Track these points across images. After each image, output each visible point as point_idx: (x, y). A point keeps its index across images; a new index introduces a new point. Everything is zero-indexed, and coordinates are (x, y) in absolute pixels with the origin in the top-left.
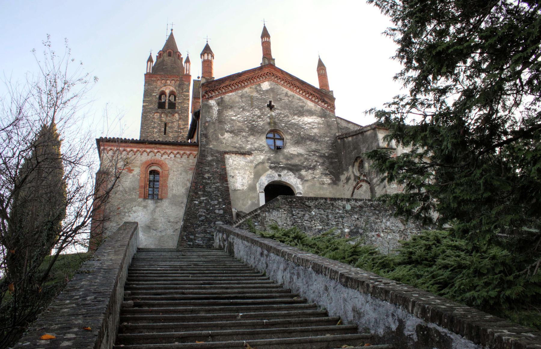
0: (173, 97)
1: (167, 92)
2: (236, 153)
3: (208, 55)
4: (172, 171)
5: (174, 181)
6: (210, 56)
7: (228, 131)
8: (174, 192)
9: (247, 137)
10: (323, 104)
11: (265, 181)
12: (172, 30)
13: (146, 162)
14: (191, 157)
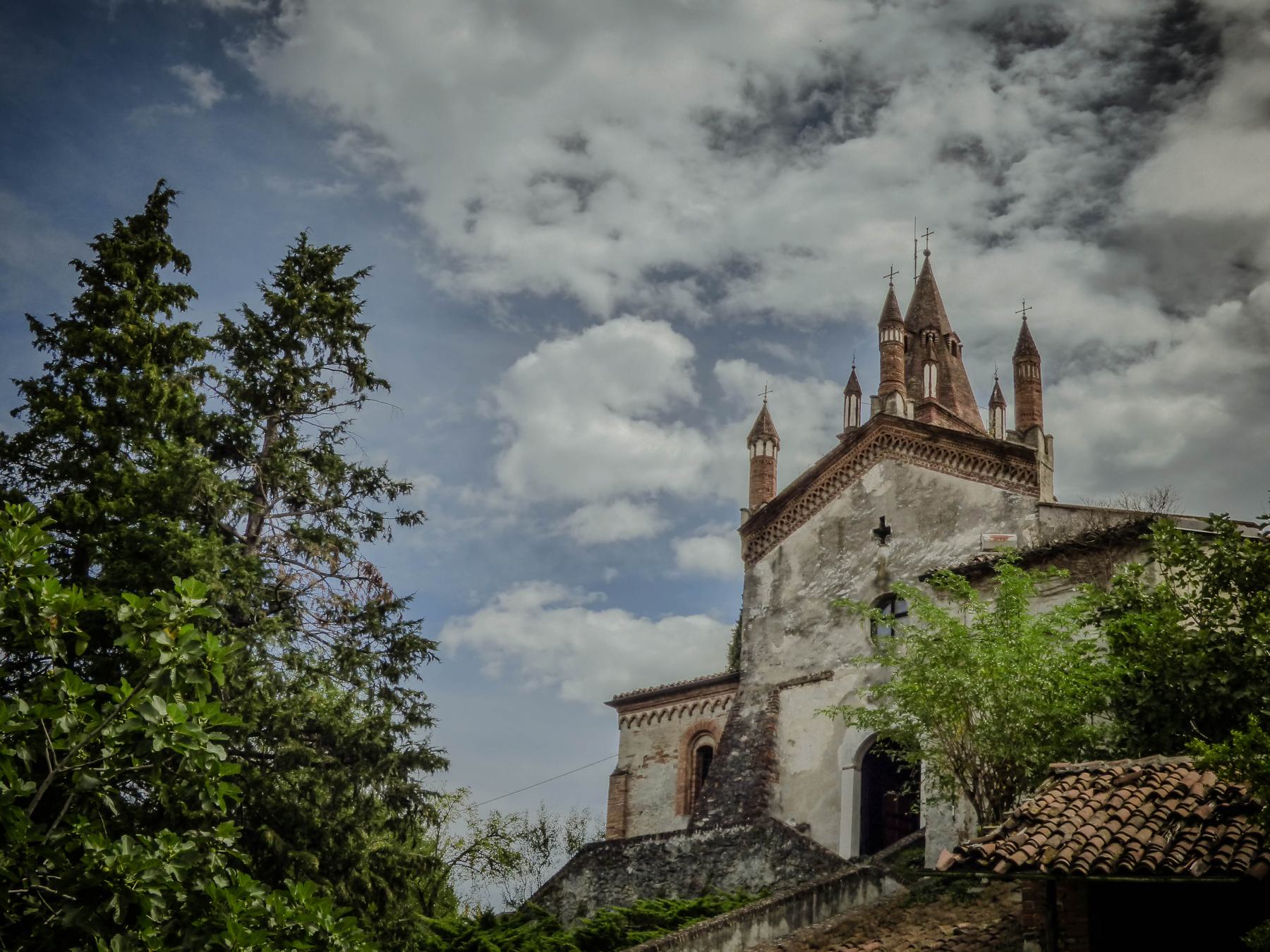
2: (803, 682)
3: (765, 444)
6: (769, 444)
9: (825, 635)
10: (1007, 478)
12: (927, 253)
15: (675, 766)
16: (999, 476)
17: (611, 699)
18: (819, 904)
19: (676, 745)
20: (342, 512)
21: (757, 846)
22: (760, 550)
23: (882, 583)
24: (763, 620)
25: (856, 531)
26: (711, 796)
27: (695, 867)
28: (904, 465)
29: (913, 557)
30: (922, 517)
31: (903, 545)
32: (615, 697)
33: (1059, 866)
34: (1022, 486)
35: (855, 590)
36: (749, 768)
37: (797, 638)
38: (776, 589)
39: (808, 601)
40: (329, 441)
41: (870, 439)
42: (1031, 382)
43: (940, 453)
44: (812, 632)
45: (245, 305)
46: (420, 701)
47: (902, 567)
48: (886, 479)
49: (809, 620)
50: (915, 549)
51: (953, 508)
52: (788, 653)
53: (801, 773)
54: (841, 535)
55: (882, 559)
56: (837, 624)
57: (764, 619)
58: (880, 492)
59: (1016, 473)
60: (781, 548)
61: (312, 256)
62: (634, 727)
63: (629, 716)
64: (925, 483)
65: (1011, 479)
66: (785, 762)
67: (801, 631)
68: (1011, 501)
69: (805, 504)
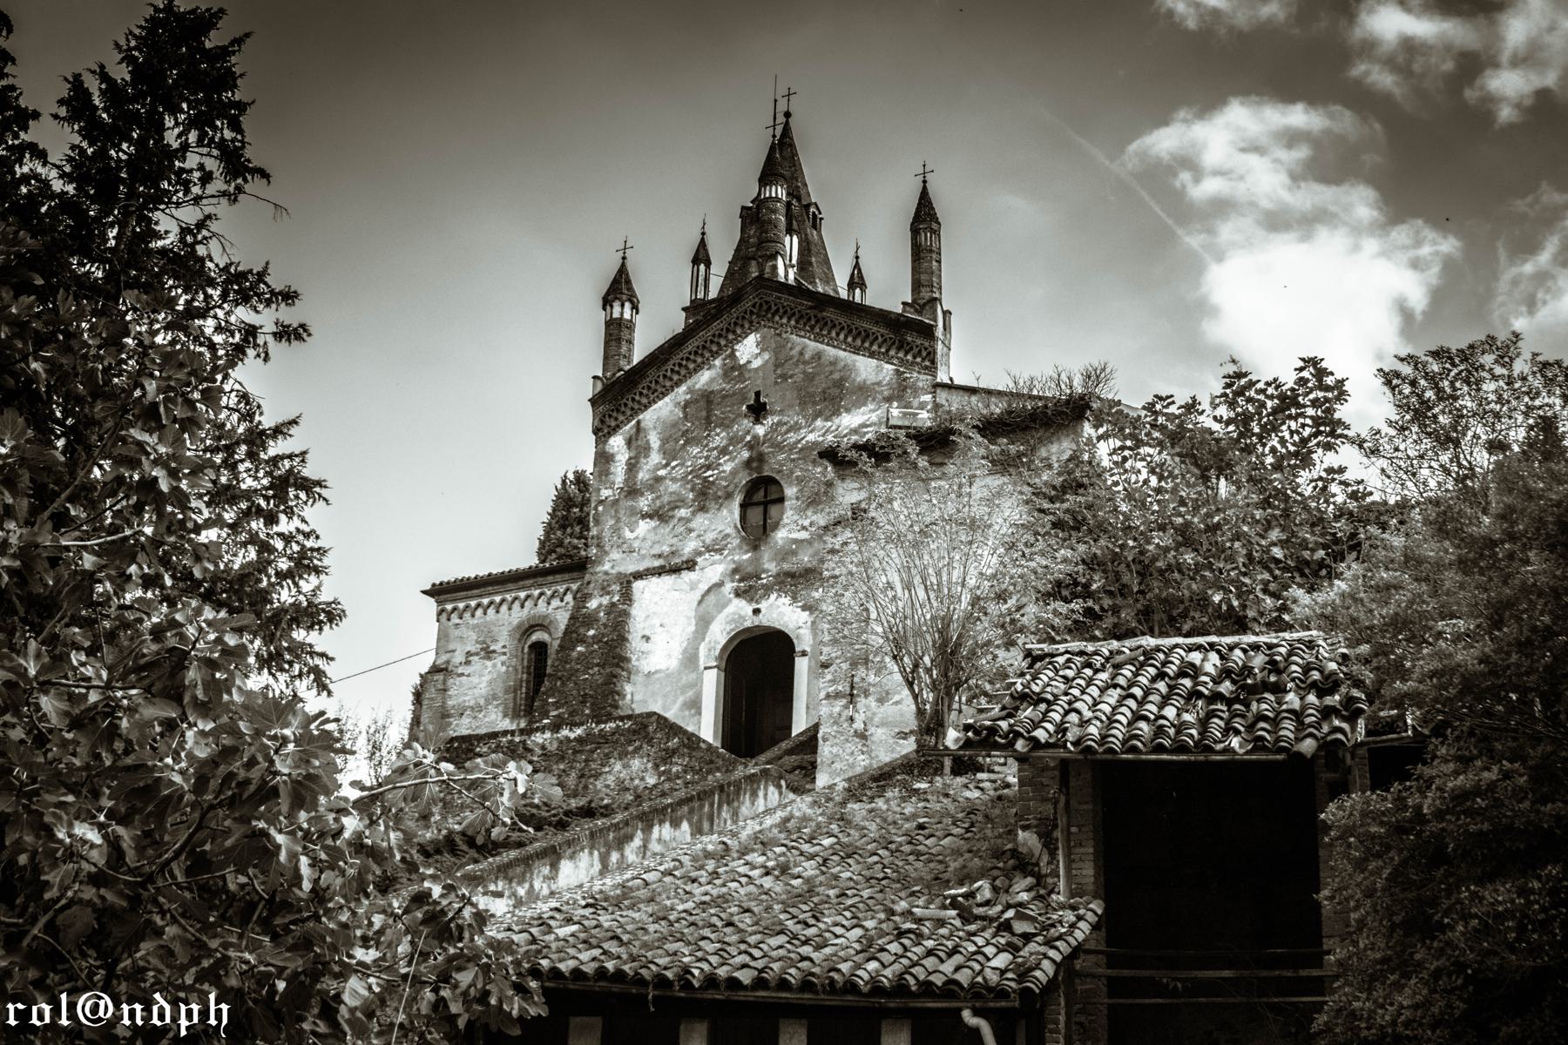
2: (659, 572)
6: (627, 305)
9: (688, 520)
11: (719, 634)
12: (787, 115)
13: (519, 626)
15: (503, 664)
16: (892, 353)
17: (428, 587)
18: (720, 806)
19: (503, 641)
20: (209, 325)
21: (637, 743)
22: (613, 424)
23: (755, 465)
24: (616, 502)
25: (726, 406)
26: (553, 696)
27: (562, 767)
28: (784, 336)
29: (792, 437)
30: (803, 393)
31: (780, 424)
32: (434, 585)
33: (1089, 743)
34: (918, 364)
35: (724, 471)
36: (598, 665)
37: (653, 523)
38: (632, 467)
39: (668, 482)
40: (189, 239)
41: (747, 304)
42: (931, 251)
43: (826, 323)
44: (673, 517)
45: (102, 67)
46: (309, 544)
47: (779, 447)
48: (763, 350)
49: (669, 503)
50: (796, 428)
51: (839, 384)
52: (644, 539)
53: (656, 672)
54: (709, 411)
55: (755, 437)
56: (702, 509)
57: (617, 500)
58: (756, 364)
59: (911, 349)
60: (639, 422)
61: (181, 17)
62: (455, 619)
63: (449, 607)
64: (807, 356)
65: (906, 355)
66: (638, 660)
67: (659, 515)
68: (905, 380)
69: (669, 374)
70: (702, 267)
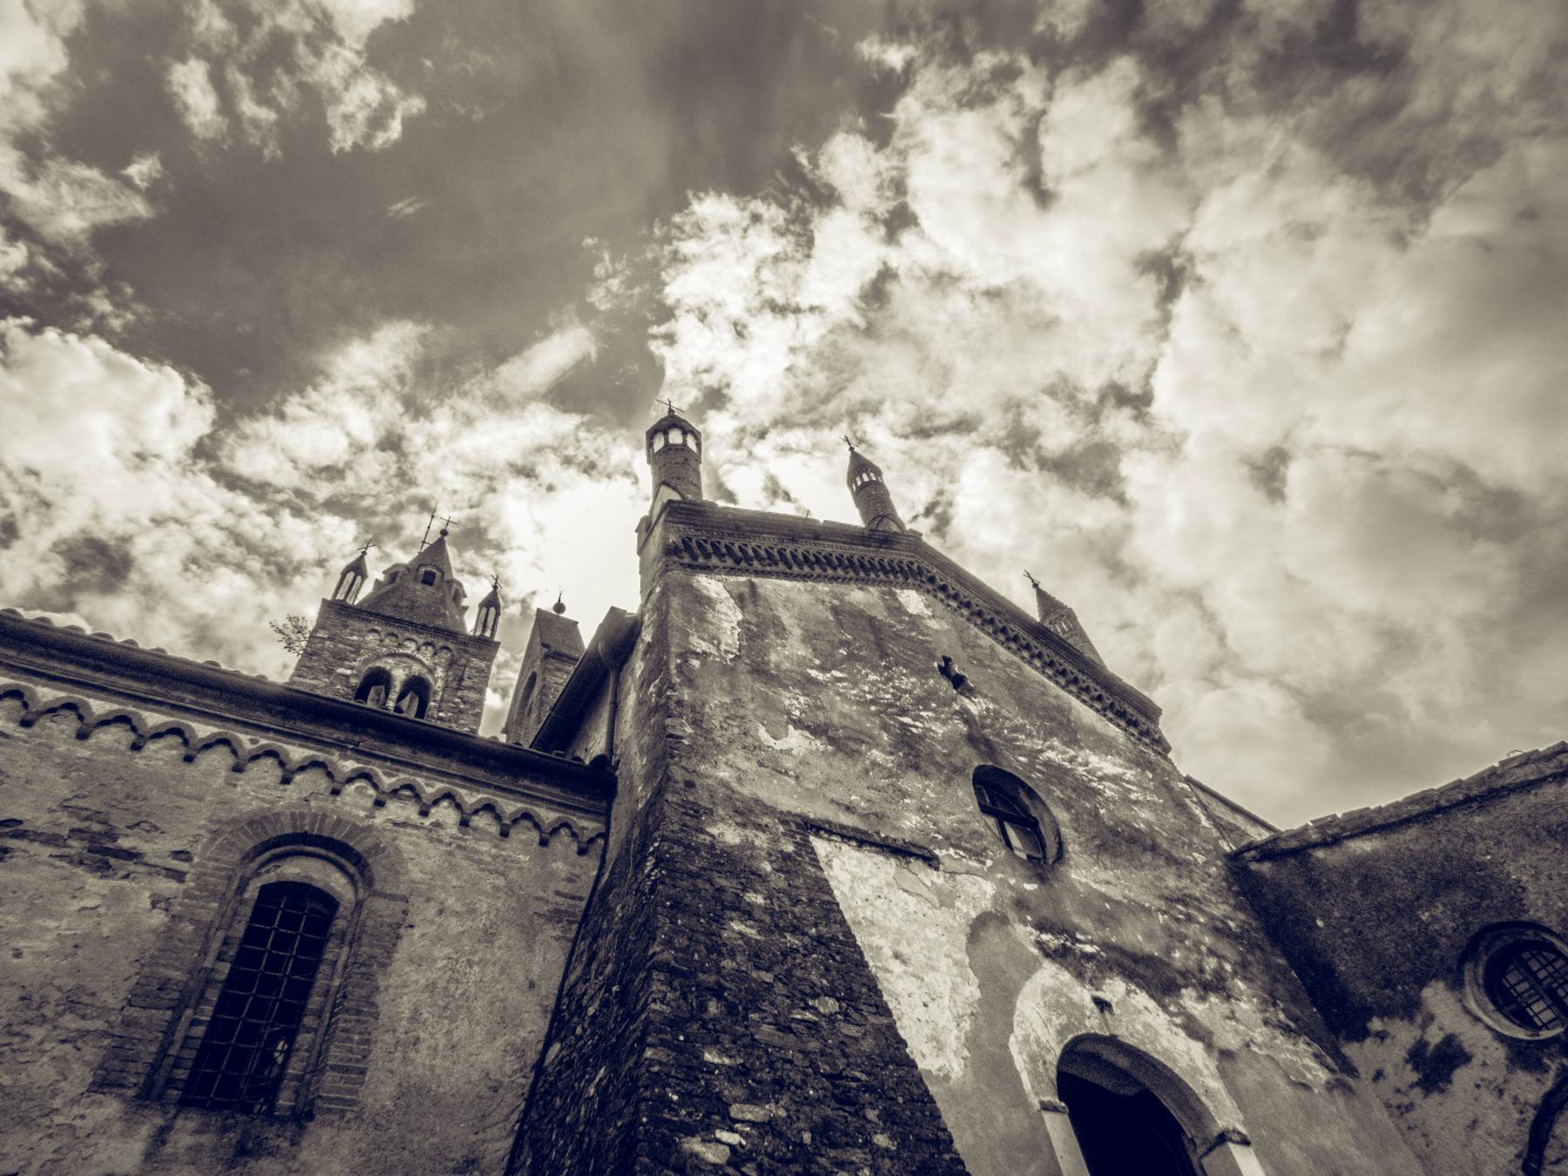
0: (416, 702)
1: (399, 675)
4: (431, 911)
5: (432, 975)
7: (800, 721)
8: (421, 1057)
13: (255, 822)
14: (563, 844)
70: (492, 610)
